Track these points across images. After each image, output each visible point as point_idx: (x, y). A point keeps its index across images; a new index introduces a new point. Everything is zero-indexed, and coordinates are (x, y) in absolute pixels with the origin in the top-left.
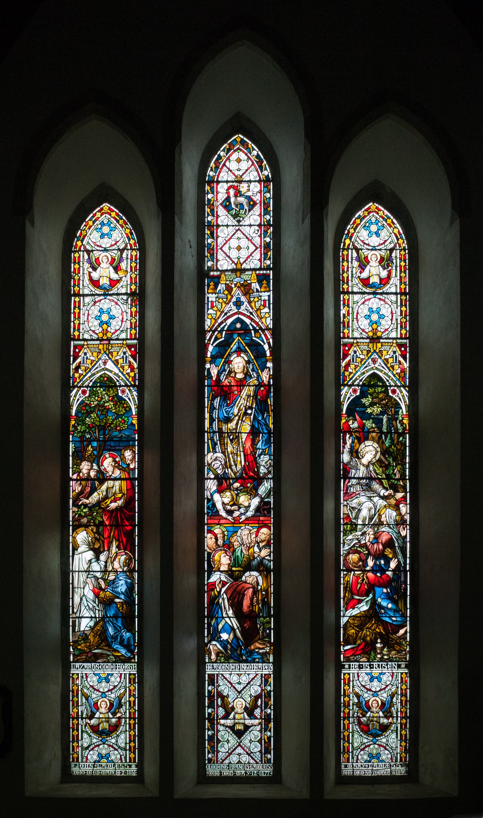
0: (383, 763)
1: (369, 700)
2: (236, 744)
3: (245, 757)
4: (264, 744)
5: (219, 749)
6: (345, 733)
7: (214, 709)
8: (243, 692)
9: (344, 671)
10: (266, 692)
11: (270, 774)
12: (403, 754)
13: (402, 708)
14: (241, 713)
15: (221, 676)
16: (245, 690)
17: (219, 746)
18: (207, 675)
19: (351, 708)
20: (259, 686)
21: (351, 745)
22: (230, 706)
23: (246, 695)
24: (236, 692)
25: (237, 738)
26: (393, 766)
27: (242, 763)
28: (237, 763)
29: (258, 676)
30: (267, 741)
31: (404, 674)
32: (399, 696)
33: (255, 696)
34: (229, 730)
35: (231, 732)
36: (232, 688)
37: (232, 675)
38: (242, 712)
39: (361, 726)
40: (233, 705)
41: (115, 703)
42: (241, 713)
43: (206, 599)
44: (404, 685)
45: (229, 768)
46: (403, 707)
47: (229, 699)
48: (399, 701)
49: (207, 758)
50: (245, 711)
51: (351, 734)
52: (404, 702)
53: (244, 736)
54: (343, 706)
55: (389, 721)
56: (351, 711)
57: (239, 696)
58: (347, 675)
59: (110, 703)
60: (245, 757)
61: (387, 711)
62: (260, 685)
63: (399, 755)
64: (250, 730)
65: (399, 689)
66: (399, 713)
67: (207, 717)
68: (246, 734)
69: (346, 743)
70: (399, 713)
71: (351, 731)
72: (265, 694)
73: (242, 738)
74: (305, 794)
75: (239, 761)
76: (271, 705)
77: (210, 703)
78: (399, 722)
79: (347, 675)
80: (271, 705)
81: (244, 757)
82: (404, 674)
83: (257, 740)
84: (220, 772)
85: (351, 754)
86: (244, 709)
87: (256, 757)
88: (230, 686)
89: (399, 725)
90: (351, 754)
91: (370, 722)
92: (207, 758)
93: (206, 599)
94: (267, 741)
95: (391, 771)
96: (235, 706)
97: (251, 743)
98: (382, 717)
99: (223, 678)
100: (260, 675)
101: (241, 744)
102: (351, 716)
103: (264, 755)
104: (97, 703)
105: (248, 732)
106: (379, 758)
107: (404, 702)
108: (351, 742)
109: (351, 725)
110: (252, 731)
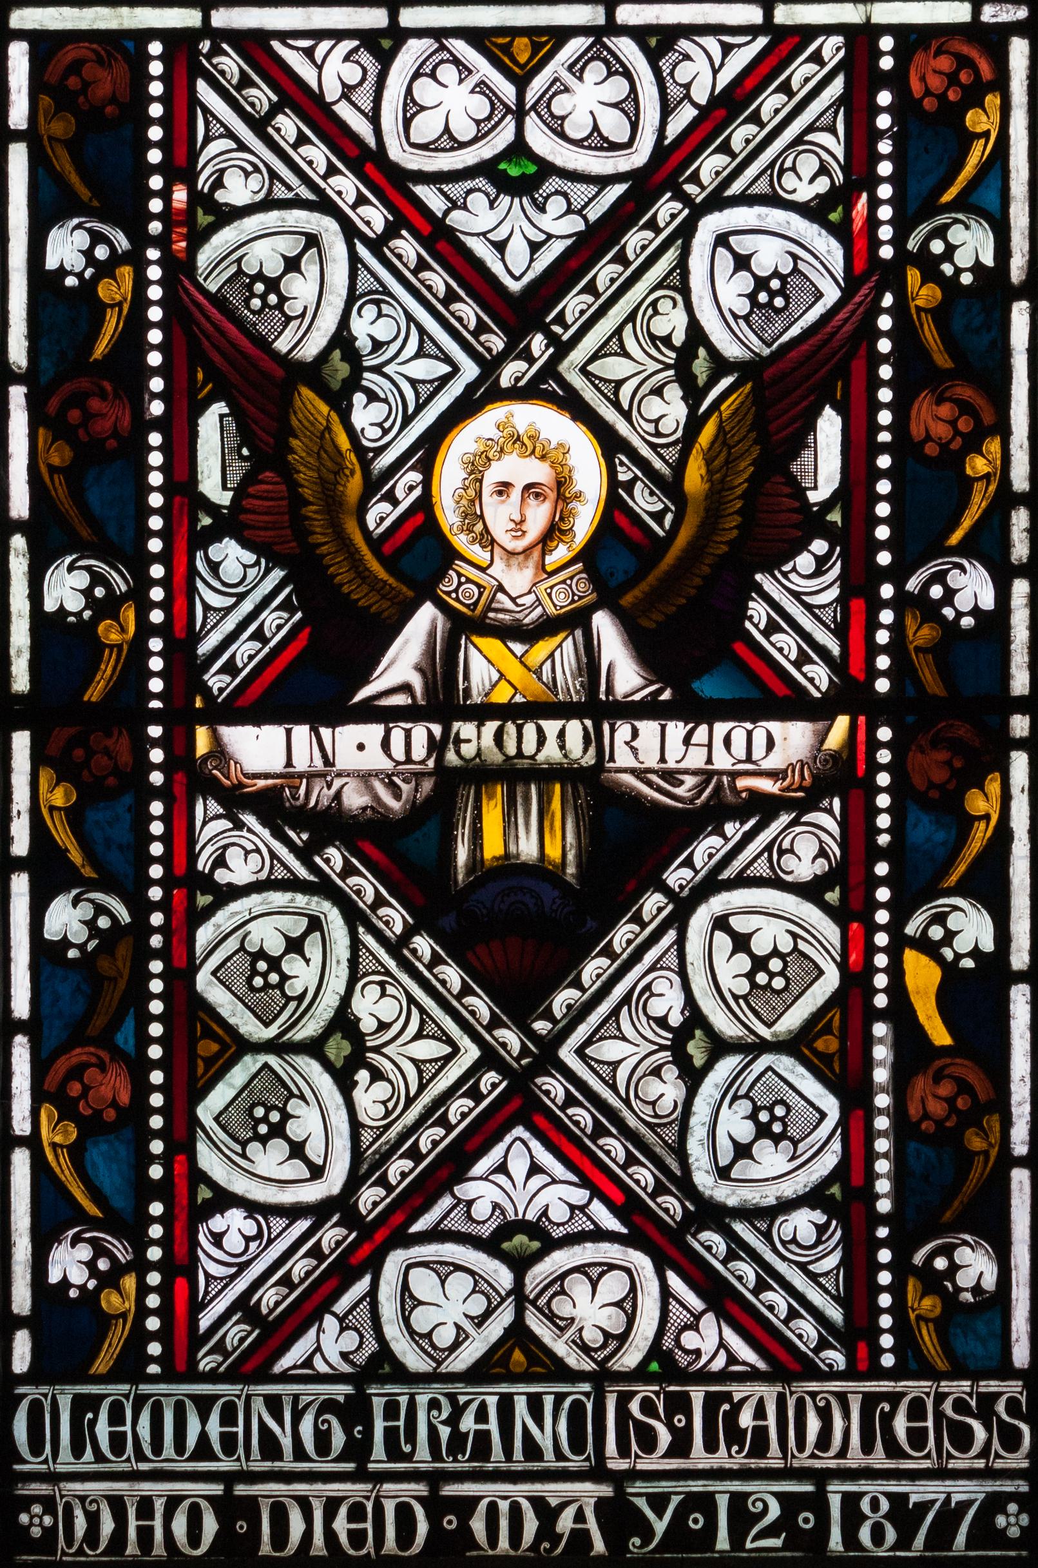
2: (467, 1085)
3: (614, 1286)
4: (900, 1085)
5: (209, 1160)
7: (138, 563)
8: (574, 304)
9: (551, 610)
10: (925, 295)
11: (983, 1533)
14: (548, 627)
15: (230, 64)
16: (605, 273)
17: (207, 1111)
18: (18, 55)
20: (814, 211)
22: (380, 516)
23: (614, 345)
24: (468, 311)
25: (481, 1006)
27: (560, 1372)
28: (479, 1373)
29: (801, 72)
30: (940, 1036)
33: (748, 370)
34: (365, 886)
35: (395, 918)
36: (407, 247)
37: (413, 51)
38: (560, 601)
40: (425, 504)
42: (548, 627)
43: (991, 1553)
45: (358, 1450)
47: (364, 416)
49: (22, 1299)
50: (607, 598)
53: (593, 969)
57: (511, 372)
60: (614, 1286)
62: (839, 197)
64: (677, 877)
68: (622, 935)
72: (904, 332)
73: (564, 999)
74: (213, 13)
75: (518, 1332)
76: (1006, 499)
77: (72, 474)
80: (1006, 499)
81: (593, 1274)
83: (793, 1019)
84: (226, 1507)
86: (587, 556)
87: (768, 1277)
88: (375, 217)
92: (22, 1299)
93: (991, 1553)
94: (940, 1036)
96: (448, 516)
97: (693, 1078)
99: (261, 96)
100: (832, 47)
101: (554, 1087)
103: (903, 1246)
105: (653, 903)
110: (710, 886)
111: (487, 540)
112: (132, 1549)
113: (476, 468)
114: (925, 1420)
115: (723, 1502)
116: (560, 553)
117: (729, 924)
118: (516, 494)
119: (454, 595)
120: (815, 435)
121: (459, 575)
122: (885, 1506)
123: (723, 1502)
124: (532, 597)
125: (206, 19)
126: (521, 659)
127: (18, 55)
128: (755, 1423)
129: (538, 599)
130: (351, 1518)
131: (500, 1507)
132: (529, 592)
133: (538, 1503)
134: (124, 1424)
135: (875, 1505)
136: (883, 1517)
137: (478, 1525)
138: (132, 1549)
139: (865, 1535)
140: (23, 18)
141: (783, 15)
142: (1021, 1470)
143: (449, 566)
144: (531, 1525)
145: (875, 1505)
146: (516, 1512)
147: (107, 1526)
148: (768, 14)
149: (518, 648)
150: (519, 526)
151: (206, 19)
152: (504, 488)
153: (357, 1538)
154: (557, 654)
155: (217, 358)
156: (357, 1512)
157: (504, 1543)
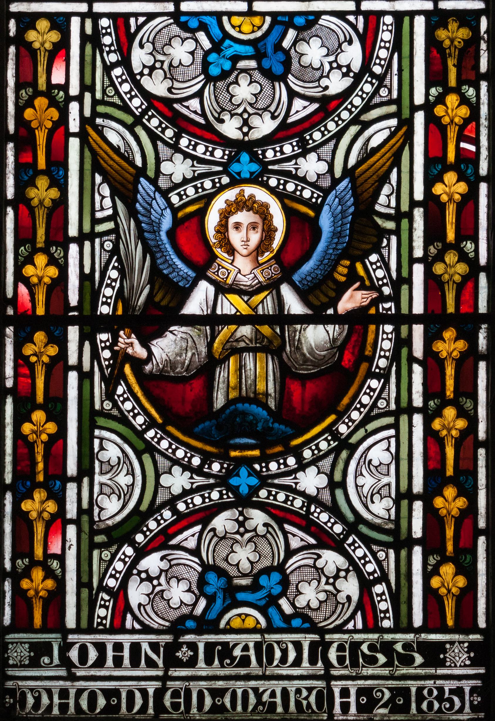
86: (277, 258)
104: (202, 213)
111: (231, 251)
112: (56, 711)
113: (225, 215)
114: (345, 652)
116: (267, 255)
119: (216, 273)
120: (91, 137)
121: (219, 265)
124: (253, 275)
126: (246, 302)
128: (242, 654)
129: (255, 276)
130: (173, 696)
131: (238, 692)
132: (251, 273)
133: (255, 690)
135: (430, 692)
136: (428, 699)
137: (227, 701)
138: (56, 711)
139: (424, 706)
140: (15, 8)
142: (320, 675)
143: (214, 261)
144: (252, 700)
145: (430, 692)
146: (245, 694)
147: (45, 700)
149: (246, 298)
152: (237, 226)
153: (176, 706)
154: (265, 300)
157: (239, 708)
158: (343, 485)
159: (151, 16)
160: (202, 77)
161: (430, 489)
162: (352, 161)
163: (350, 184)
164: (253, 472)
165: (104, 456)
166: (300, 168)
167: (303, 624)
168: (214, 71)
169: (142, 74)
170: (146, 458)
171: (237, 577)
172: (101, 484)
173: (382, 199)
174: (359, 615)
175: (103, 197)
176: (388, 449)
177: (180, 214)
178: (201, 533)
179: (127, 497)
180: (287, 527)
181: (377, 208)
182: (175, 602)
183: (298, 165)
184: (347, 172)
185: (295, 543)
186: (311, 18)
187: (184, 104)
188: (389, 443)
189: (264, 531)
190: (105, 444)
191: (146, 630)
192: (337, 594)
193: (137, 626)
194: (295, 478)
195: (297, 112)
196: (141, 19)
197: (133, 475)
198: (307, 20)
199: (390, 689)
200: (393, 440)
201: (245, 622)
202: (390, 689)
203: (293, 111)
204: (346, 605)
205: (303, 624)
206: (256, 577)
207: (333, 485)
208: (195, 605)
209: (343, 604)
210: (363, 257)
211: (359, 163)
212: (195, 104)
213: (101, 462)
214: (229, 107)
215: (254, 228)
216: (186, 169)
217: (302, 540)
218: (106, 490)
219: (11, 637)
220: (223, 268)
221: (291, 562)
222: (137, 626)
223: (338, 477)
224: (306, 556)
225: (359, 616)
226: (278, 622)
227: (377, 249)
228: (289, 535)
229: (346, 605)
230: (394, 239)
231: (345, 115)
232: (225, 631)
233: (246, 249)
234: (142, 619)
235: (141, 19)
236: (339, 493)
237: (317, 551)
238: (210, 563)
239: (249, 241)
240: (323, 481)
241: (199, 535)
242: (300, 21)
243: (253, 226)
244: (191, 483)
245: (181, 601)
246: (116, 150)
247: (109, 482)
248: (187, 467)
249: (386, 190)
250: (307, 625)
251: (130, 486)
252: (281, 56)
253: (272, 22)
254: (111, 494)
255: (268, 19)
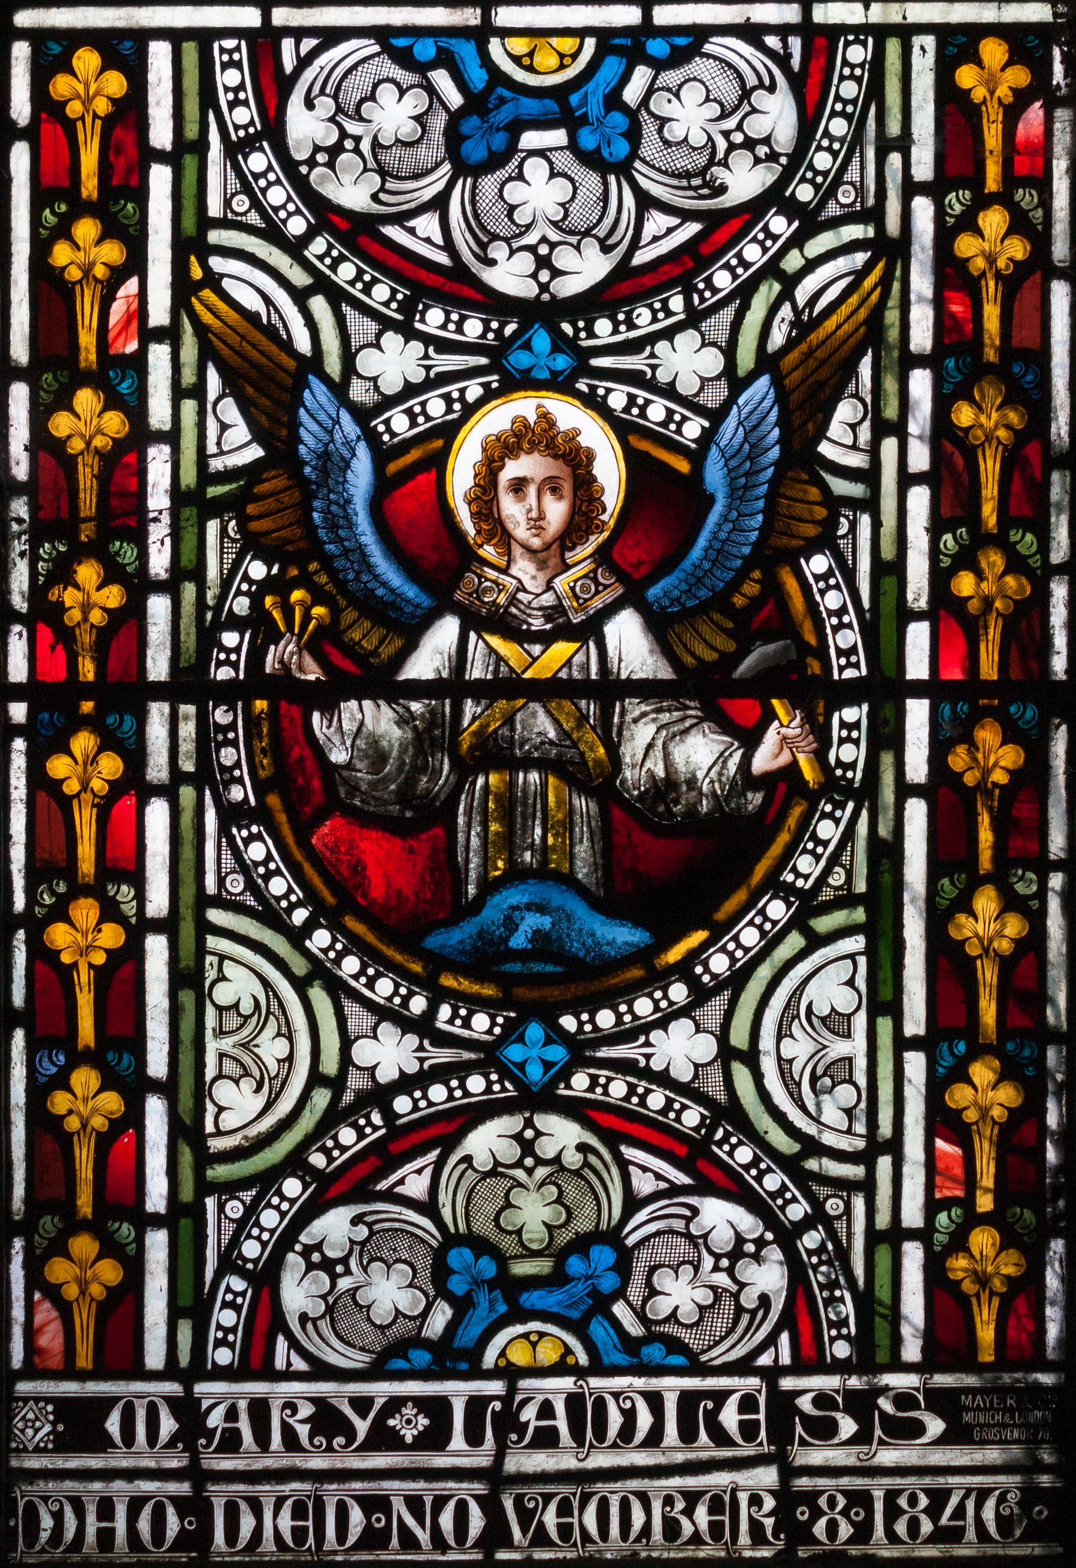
0: (671, 1386)
1: (448, 431)
6: (59, 935)
12: (982, 1240)
13: (966, 560)
19: (159, 562)
21: (155, 1108)
26: (824, 1430)
31: (993, 51)
32: (921, 383)
39: (324, 834)
41: (714, 475)
44: (993, 220)
46: (980, 540)
48: (920, 458)
51: (156, 947)
52: (990, 468)
54: (37, 533)
55: (764, 759)
56: (158, 606)
58: (87, 60)
59: (635, 462)
61: (721, 601)
63: (913, 1255)
65: (921, 283)
66: (918, 635)
67: (18, 998)
69: (85, 1079)
70: (918, 635)
71: (158, 902)
78: (917, 768)
79: (87, 60)
82: (993, 51)
85: (157, 1243)
89: (916, 811)
90: (157, 1243)
91: (465, 769)
95: (785, 1496)
98: (645, 689)
102: (158, 668)
104: (438, 462)
106: (601, 1304)
107: (990, 468)
108: (157, 1065)
109: (157, 814)
111: (501, 535)
115: (878, 1494)
117: (210, 923)
118: (532, 491)
122: (924, 1501)
123: (878, 1494)
125: (647, 16)
127: (21, 51)
134: (757, 1412)
141: (821, 14)
148: (807, 13)
150: (537, 522)
151: (647, 16)
152: (519, 486)
153: (299, 1534)
155: (225, 351)
156: (299, 1511)
158: (751, 1058)
159: (332, 36)
160: (630, 1241)
161: (941, 1070)
162: (778, 338)
163: (772, 390)
164: (519, 338)
165: (223, 994)
166: (414, 1051)
167: (411, 47)
168: (603, 1256)
169: (312, 163)
170: (318, 996)
171: (516, 1257)
172: (222, 1056)
173: (836, 429)
174: (784, 1338)
175: (224, 427)
176: (851, 983)
177: (393, 468)
178: (635, 245)
179: (278, 1083)
180: (442, 258)
181: (825, 449)
182: (382, 1314)
183: (417, 1058)
184: (766, 361)
185: (428, 224)
186: (682, 41)
187: (666, 1185)
188: (219, 444)
189: (492, 249)
190: (229, 968)
191: (321, 1371)
192: (336, 114)
193: (299, 1364)
194: (648, 1044)
195: (419, 1172)
196: (308, 44)
197: (290, 1038)
198: (674, 47)
199: (845, 1493)
200: (212, 448)
201: (538, 1348)
202: (845, 1493)
203: (428, 1172)
204: (316, 90)
205: (411, 47)
206: (561, 1256)
207: (726, 1053)
208: (650, 91)
209: (322, 92)
210: (793, 558)
211: (791, 344)
212: (428, 224)
213: (220, 1009)
214: (503, 228)
215: (554, 490)
216: (665, 1046)
217: (412, 231)
218: (229, 1067)
219: (23, 1387)
220: (487, 580)
221: (440, 186)
222: (299, 1364)
223: (739, 1038)
224: (408, 197)
225: (289, 63)
226: (466, 51)
227: (826, 541)
228: (631, 1168)
229: (316, 90)
230: (865, 520)
231: (752, 253)
232: (582, 33)
233: (537, 535)
234: (311, 1349)
235: (308, 44)
236: (741, 1075)
237: (382, 209)
238: (461, 1231)
239: (543, 519)
240: (706, 1048)
241: (434, 1170)
242: (421, 1358)
243: (551, 485)
244: (418, 1058)
245: (396, 1309)
246: (252, 317)
247: (237, 1052)
248: (406, 1024)
249: (845, 411)
250: (401, 42)
251: (284, 1061)
252: (618, 120)
253: (598, 46)
254: (241, 1077)
255: (590, 43)
